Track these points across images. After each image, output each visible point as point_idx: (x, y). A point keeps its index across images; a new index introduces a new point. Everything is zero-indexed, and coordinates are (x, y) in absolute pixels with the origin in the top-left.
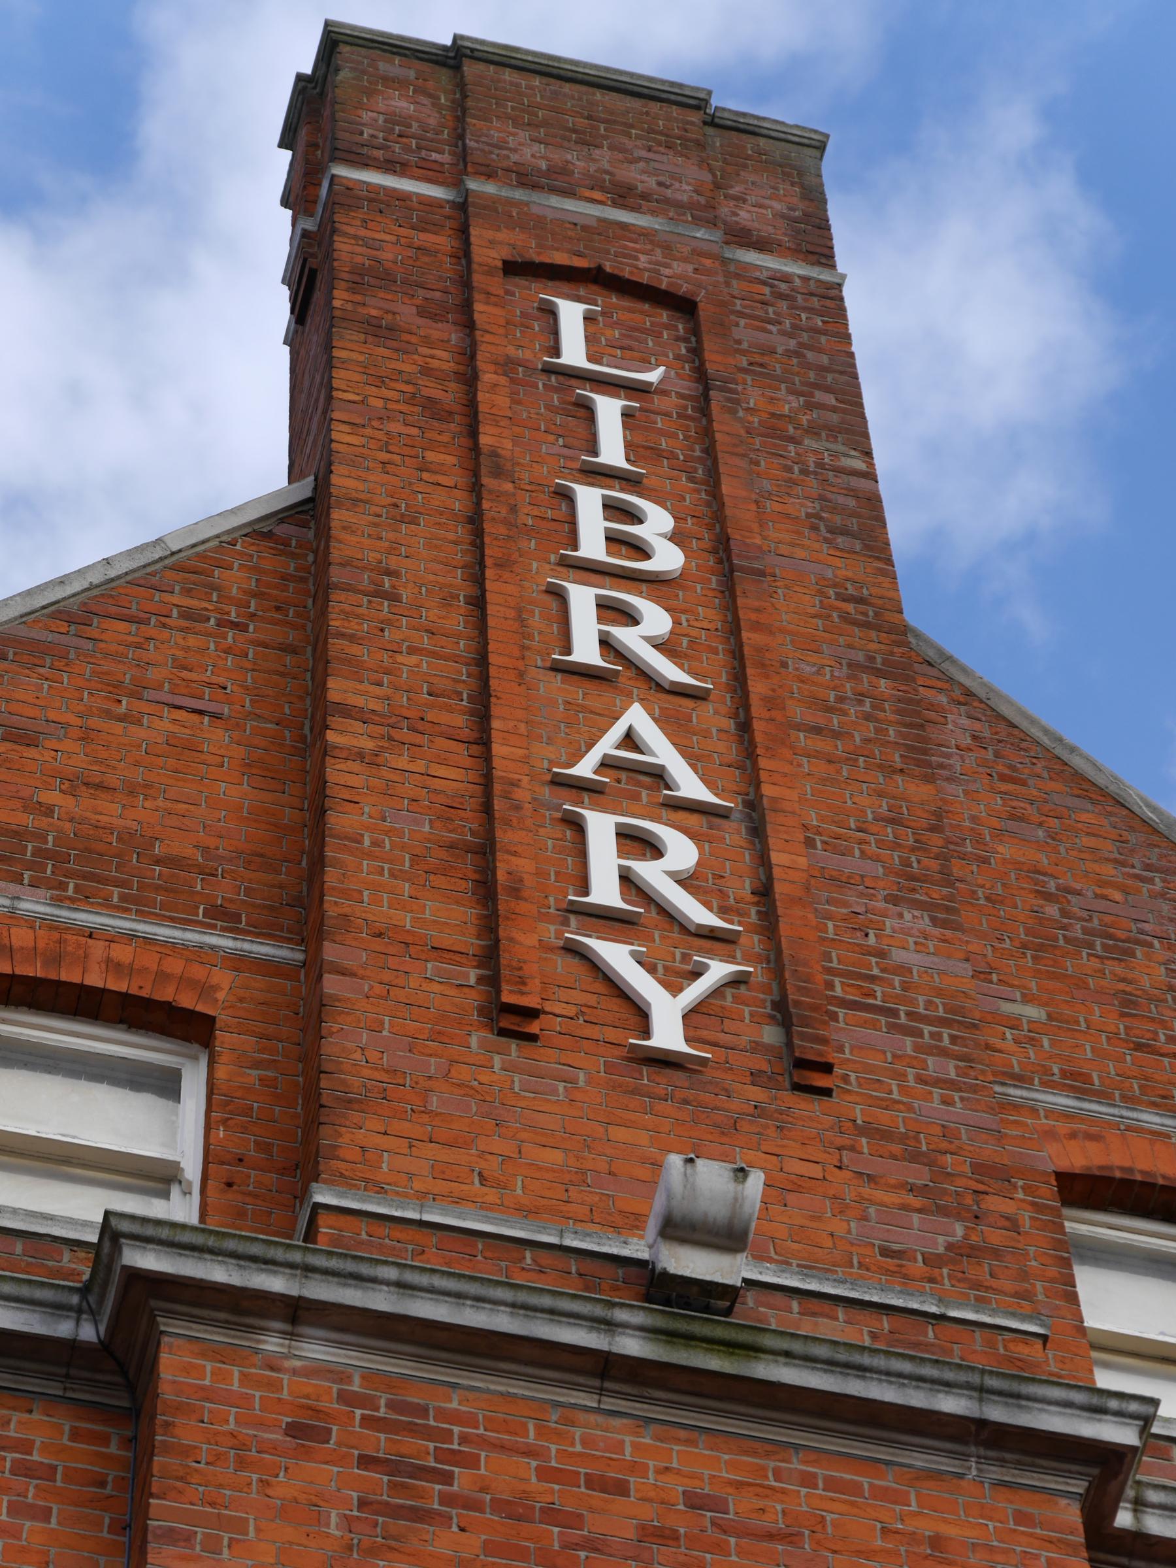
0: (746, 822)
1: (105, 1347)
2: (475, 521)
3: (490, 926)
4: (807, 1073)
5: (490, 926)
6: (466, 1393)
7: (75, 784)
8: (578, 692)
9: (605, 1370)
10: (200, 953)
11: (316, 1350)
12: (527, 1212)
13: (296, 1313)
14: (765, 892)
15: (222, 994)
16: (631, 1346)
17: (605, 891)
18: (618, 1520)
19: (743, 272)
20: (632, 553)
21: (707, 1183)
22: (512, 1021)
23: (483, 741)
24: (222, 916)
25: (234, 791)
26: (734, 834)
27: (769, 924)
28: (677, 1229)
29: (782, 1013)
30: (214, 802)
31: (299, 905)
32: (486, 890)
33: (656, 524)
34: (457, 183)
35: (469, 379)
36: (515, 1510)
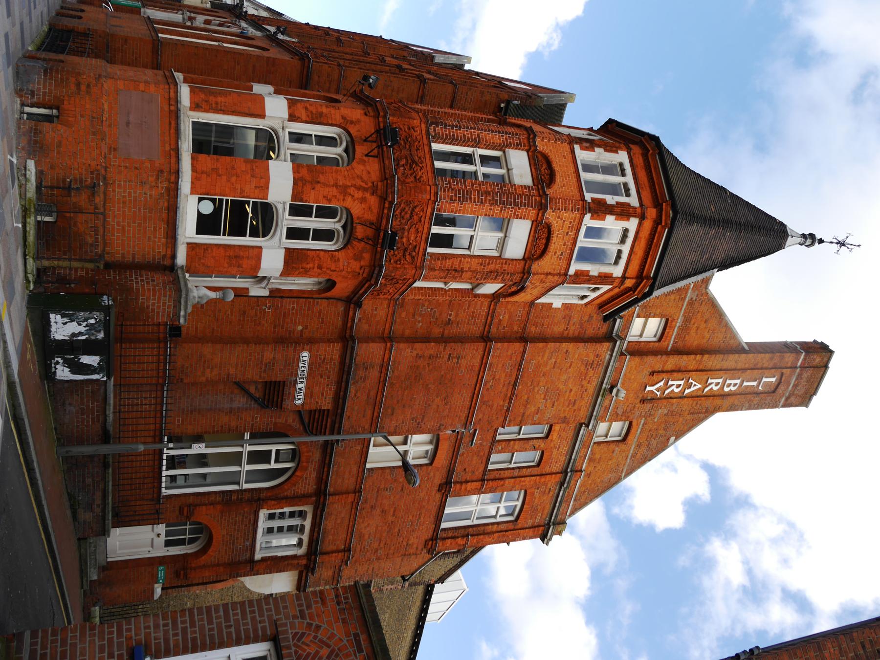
0: (681, 397)
1: (611, 336)
2: (735, 369)
3: (667, 372)
4: (643, 401)
5: (667, 372)
6: (601, 370)
7: (698, 328)
8: (705, 380)
9: (602, 383)
10: (670, 341)
11: (608, 357)
12: (625, 375)
13: (611, 355)
14: (671, 398)
15: (663, 344)
16: (604, 386)
17: (671, 383)
18: (585, 383)
19: (781, 397)
20: (694, 394)
21: (622, 394)
22: (652, 373)
23: (697, 371)
24: (675, 342)
25: (696, 343)
26: (680, 395)
27: (665, 398)
28: (618, 390)
29: (652, 399)
30: (693, 340)
31: (677, 351)
32: (672, 371)
33: (733, 389)
34: (800, 367)
35: (761, 369)
36: (586, 374)
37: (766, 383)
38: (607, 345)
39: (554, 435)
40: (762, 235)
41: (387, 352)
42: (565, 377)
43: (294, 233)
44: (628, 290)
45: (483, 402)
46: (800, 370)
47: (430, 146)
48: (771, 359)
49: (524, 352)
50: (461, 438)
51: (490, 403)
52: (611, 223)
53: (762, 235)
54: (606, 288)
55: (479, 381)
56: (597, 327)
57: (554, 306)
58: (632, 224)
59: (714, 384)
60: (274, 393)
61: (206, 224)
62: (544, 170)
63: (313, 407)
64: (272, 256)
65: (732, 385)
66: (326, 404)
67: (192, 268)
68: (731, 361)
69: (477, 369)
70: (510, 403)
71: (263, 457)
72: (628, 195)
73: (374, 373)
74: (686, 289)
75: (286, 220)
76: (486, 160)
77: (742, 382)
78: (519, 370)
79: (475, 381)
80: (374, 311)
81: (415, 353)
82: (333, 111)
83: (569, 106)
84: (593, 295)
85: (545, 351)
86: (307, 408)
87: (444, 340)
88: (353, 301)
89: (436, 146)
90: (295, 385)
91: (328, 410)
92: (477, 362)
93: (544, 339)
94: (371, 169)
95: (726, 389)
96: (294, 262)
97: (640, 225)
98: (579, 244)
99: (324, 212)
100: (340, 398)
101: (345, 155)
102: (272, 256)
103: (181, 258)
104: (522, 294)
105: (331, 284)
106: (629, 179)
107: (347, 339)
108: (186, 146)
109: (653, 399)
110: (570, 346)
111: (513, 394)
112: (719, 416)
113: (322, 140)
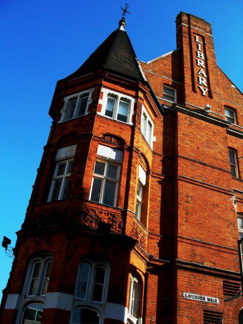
37: (199, 40)
41: (184, 240)
42: (199, 137)
43: (97, 295)
44: (145, 96)
45: (216, 183)
47: (49, 203)
48: (185, 37)
49: (184, 158)
50: (239, 199)
51: (217, 179)
54: (144, 110)
55: (202, 185)
57: (155, 140)
63: (222, 292)
66: (220, 282)
69: (194, 186)
70: (216, 168)
72: (88, 94)
73: (198, 250)
77: (199, 50)
78: (195, 162)
79: (203, 188)
81: (185, 224)
84: (149, 118)
85: (183, 146)
86: (222, 296)
89: (49, 200)
90: (206, 303)
91: (224, 281)
92: (190, 186)
95: (203, 58)
97: (105, 87)
98: (116, 119)
101: (46, 258)
104: (147, 156)
106: (79, 94)
111: (210, 166)
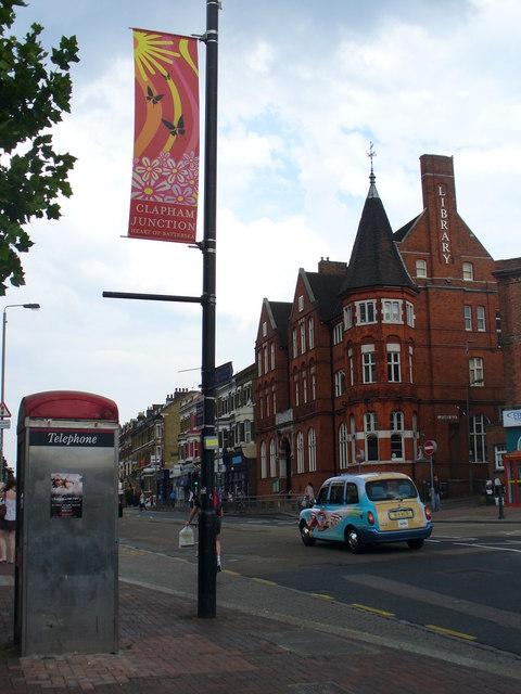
31: (430, 250)
38: (430, 290)
39: (469, 302)
40: (374, 210)
43: (399, 429)
46: (437, 174)
52: (385, 311)
53: (374, 210)
56: (422, 296)
58: (383, 301)
59: (444, 225)
60: (452, 426)
61: (399, 455)
62: (368, 339)
64: (408, 434)
65: (444, 214)
67: (413, 459)
68: (433, 219)
71: (479, 427)
74: (403, 255)
75: (395, 431)
76: (367, 361)
80: (422, 393)
82: (133, 669)
83: (270, 300)
87: (431, 364)
88: (419, 402)
93: (429, 320)
94: (377, 405)
96: (408, 427)
99: (392, 419)
100: (455, 403)
102: (408, 434)
103: (410, 462)
105: (415, 412)
107: (432, 402)
108: (376, 462)
109: (452, 258)
110: (431, 308)
112: (463, 210)
113: (369, 421)
